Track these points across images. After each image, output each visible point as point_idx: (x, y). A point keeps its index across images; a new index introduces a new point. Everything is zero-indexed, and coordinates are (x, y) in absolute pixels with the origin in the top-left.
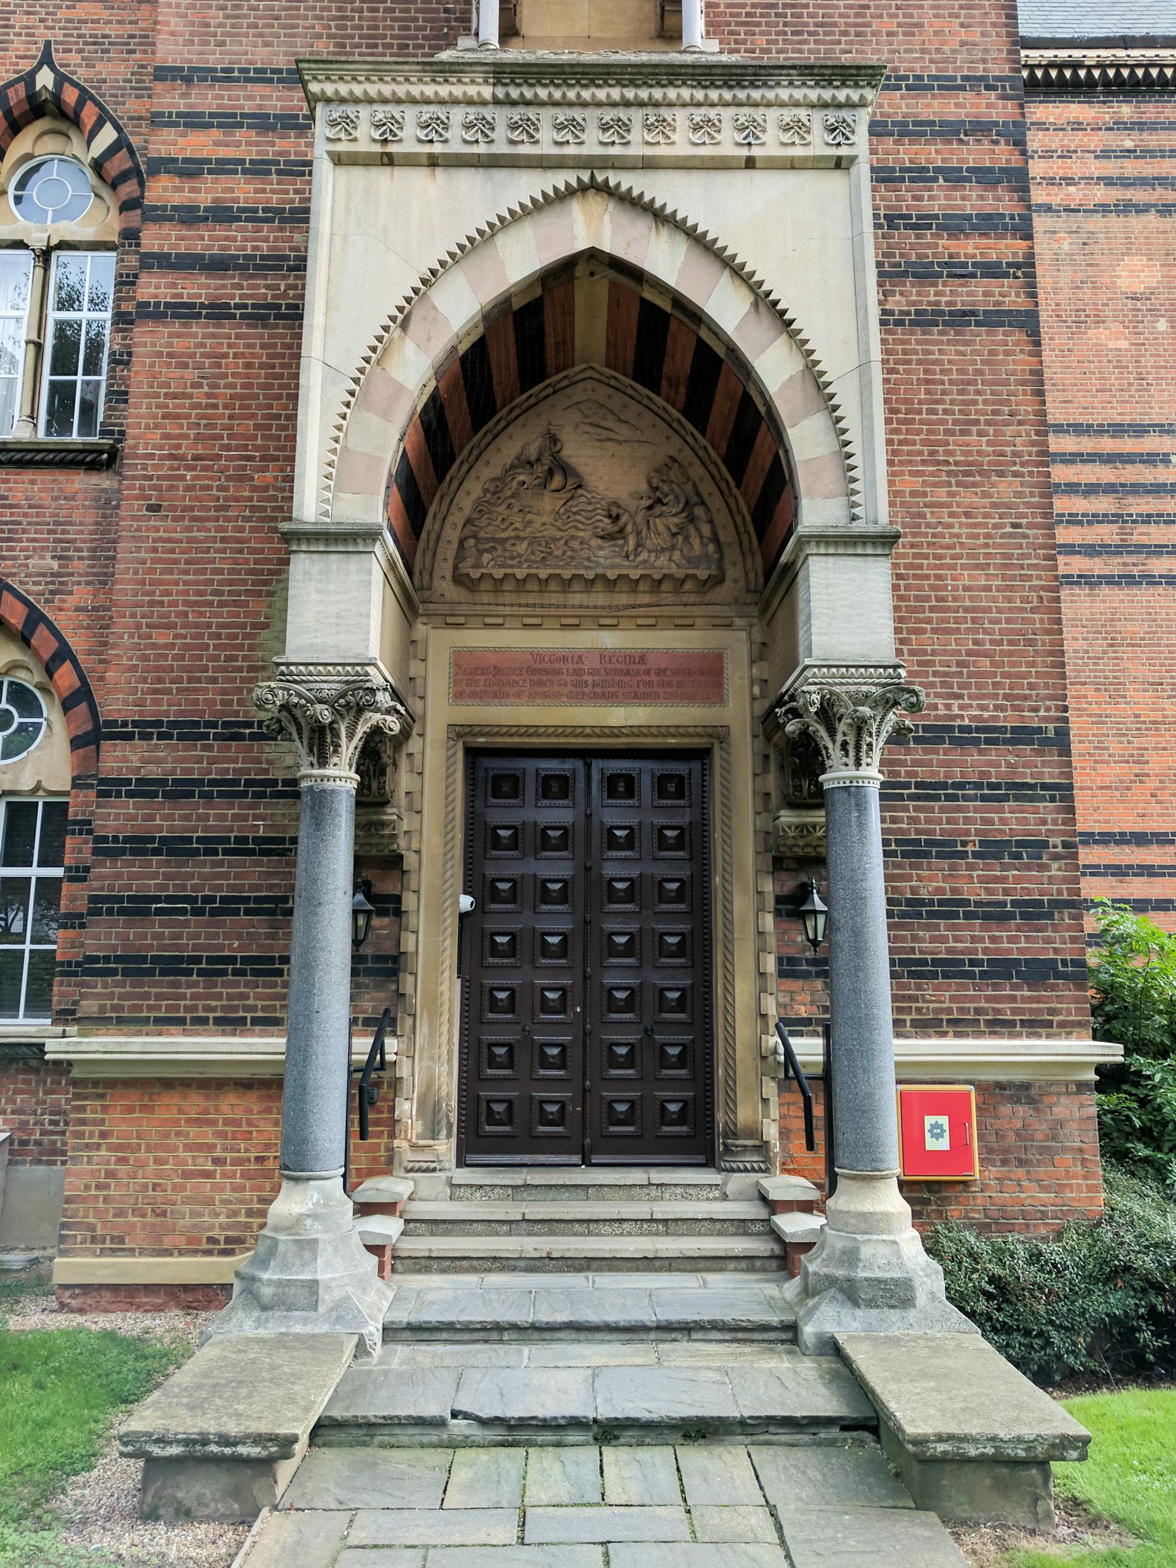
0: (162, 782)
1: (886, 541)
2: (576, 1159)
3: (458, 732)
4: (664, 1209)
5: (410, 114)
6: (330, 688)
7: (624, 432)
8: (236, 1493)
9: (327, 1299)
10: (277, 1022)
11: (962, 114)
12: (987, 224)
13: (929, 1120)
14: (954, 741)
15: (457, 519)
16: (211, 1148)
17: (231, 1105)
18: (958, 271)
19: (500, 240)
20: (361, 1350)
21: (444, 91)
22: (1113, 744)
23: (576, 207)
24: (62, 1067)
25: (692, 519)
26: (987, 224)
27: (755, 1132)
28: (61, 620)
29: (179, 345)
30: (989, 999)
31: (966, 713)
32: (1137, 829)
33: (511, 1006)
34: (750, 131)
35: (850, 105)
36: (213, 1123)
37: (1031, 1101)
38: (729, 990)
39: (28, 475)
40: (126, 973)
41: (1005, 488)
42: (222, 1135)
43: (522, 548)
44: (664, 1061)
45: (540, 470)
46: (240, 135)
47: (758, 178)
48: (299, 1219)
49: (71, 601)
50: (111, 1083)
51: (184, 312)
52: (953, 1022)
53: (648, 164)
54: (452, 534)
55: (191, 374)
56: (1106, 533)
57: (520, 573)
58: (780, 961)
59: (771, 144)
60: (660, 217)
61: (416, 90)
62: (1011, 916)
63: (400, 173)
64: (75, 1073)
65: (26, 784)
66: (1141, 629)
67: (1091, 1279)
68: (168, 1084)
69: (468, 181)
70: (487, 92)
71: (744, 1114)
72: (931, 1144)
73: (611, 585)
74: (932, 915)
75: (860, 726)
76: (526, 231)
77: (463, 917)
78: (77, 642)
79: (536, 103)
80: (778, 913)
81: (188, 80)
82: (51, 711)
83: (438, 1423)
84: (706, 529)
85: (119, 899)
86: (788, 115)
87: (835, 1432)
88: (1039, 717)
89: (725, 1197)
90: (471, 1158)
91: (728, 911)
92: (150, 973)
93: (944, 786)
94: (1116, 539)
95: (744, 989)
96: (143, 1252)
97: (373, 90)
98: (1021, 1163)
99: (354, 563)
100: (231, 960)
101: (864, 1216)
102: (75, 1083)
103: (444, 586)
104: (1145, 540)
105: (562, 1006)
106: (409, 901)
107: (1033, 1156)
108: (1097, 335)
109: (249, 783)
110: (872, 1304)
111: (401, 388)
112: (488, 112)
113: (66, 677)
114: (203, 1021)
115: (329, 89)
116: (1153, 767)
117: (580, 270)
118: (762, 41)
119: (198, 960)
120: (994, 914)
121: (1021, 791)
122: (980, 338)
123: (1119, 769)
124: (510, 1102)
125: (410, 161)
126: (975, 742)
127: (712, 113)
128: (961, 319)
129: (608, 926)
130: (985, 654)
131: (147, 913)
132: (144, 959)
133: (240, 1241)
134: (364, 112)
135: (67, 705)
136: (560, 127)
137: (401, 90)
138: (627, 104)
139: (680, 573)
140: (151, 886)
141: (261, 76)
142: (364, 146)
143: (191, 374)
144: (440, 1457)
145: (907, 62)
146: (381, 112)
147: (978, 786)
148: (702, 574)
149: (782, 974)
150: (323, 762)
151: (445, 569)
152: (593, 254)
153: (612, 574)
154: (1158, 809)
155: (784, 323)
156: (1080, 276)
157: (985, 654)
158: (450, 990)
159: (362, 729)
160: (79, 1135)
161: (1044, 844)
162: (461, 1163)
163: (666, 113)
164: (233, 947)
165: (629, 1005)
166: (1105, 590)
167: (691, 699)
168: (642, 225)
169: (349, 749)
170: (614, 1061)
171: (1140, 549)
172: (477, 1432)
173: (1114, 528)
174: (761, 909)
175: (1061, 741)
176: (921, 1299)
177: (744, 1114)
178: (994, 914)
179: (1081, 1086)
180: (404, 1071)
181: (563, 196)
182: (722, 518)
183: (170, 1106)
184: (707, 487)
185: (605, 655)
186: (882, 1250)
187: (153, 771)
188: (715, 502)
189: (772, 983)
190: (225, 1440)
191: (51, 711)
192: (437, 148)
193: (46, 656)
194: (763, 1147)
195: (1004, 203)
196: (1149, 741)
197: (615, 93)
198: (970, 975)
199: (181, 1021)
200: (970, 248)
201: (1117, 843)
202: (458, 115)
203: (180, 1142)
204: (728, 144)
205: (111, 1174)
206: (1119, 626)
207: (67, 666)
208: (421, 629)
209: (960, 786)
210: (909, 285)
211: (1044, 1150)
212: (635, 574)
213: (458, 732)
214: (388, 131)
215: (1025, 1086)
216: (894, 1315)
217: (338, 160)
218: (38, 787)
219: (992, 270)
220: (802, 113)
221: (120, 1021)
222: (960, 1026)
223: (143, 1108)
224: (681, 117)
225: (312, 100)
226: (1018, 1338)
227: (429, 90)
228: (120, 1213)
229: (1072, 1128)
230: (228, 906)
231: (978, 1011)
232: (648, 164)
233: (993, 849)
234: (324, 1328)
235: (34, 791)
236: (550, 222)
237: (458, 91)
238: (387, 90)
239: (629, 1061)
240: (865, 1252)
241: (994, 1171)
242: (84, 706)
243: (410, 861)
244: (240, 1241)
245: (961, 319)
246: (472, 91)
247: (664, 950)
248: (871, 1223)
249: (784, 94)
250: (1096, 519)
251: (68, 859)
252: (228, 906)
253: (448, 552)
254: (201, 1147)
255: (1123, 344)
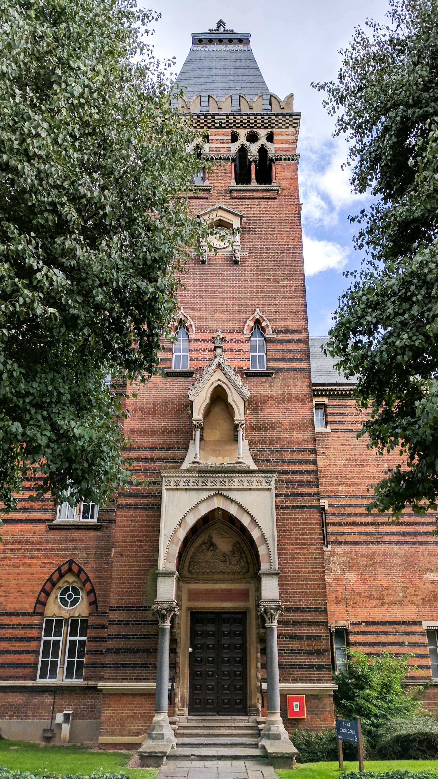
0: (123, 621)
1: (277, 574)
2: (216, 713)
3: (189, 608)
4: (234, 725)
5: (182, 480)
6: (166, 607)
7: (227, 535)
8: (157, 763)
9: (165, 738)
10: (155, 679)
11: (303, 457)
12: (309, 484)
13: (295, 703)
14: (301, 611)
15: (189, 557)
16: (133, 710)
17: (138, 700)
18: (302, 495)
19: (200, 506)
20: (173, 747)
21: (188, 475)
22: (374, 593)
23: (215, 498)
24: (101, 690)
25: (242, 557)
26: (309, 484)
27: (256, 706)
28: (87, 570)
29: (127, 515)
30: (309, 674)
31: (303, 604)
32: (382, 620)
33: (201, 675)
34: (250, 483)
35: (270, 477)
36: (134, 704)
37: (319, 699)
38: (250, 672)
39: (80, 532)
40: (115, 667)
41: (313, 549)
42: (136, 707)
43: (203, 564)
44: (236, 689)
45: (208, 545)
46: (141, 464)
47: (252, 492)
48: (160, 721)
49: (90, 566)
50: (111, 694)
51: (128, 507)
52: (301, 680)
53: (230, 490)
54: (188, 561)
55: (129, 522)
56: (371, 528)
57: (203, 571)
58: (262, 664)
59: (254, 486)
60: (233, 501)
61: (183, 475)
62: (314, 653)
63: (180, 492)
64: (104, 692)
65: (77, 614)
66: (382, 558)
67: (329, 741)
68: (124, 694)
69: (193, 493)
70: (197, 475)
71: (253, 702)
72: (295, 709)
73: (223, 573)
74: (296, 653)
75: (272, 615)
76: (205, 504)
77: (190, 653)
78: (91, 576)
79: (207, 477)
80: (261, 653)
81: (129, 451)
82: (82, 595)
83: (189, 756)
84: (245, 560)
85: (113, 649)
86: (258, 479)
87: (260, 758)
88: (320, 605)
89: (249, 722)
90: (192, 713)
91: (250, 652)
92: (120, 667)
93: (298, 622)
94: (374, 530)
95: (253, 671)
96: (118, 736)
97: (174, 475)
98: (316, 714)
99: (170, 579)
100: (138, 664)
101: (272, 721)
102: (103, 694)
103: (186, 573)
104: (382, 530)
105: (212, 675)
106: (178, 650)
107: (319, 713)
108: (367, 468)
109: (143, 621)
110: (272, 739)
111: (179, 539)
112: (197, 479)
113: (88, 586)
114: (132, 679)
115: (166, 475)
116: (386, 601)
117: (216, 511)
118: (258, 440)
119: (130, 664)
120: (310, 653)
121: (316, 623)
122: (307, 511)
123: (376, 601)
124: (200, 699)
125: (182, 489)
126: (306, 611)
127: (243, 479)
128: (303, 507)
129: (223, 656)
130: (308, 589)
131: (119, 653)
132: (118, 664)
133: (139, 733)
134: (172, 479)
135: (88, 594)
136: (212, 482)
137: (180, 475)
138: (225, 477)
139: (238, 570)
140: (120, 646)
141: (146, 450)
142: (172, 487)
143: (129, 522)
144: (190, 762)
145: (292, 445)
146: (176, 479)
147: (306, 622)
148: (244, 571)
149: (262, 668)
150: (164, 622)
151: (186, 569)
152: (219, 508)
153: (224, 571)
154: (388, 614)
155: (257, 524)
156: (362, 451)
157: (308, 589)
158: (187, 671)
159: (171, 615)
160: (104, 707)
161: (321, 636)
162: (189, 715)
163: (233, 479)
164: (139, 661)
165: (228, 675)
166: (371, 546)
167: (242, 601)
168: (228, 502)
169: (169, 619)
170: (224, 689)
171: (381, 533)
172: (196, 758)
173: (373, 527)
174: (257, 652)
175: (325, 611)
176: (282, 738)
177: (253, 702)
178: (310, 653)
179: (330, 695)
180: (177, 691)
181: (212, 496)
182: (249, 556)
183: (125, 700)
184: (245, 549)
185: (223, 590)
186: (275, 728)
187: (121, 618)
188: (247, 552)
189: (260, 670)
190: (155, 753)
191: (82, 595)
192: (187, 487)
193: (83, 580)
194: (257, 710)
195: (312, 479)
196: (385, 593)
197: (223, 475)
198: (304, 668)
199: (127, 679)
200: (305, 490)
201: (377, 625)
202: (191, 480)
203: (127, 709)
204: (246, 485)
205: (111, 716)
206: (376, 557)
207: (88, 583)
208: (181, 584)
209: (302, 622)
210: (291, 499)
211: (322, 711)
212: (229, 571)
213: (189, 608)
214: (177, 483)
215: (317, 695)
216: (277, 741)
217: (167, 489)
218: (80, 615)
219: (310, 495)
220: (261, 479)
221: (113, 679)
222: (302, 681)
223: (119, 700)
224: (236, 480)
225: (162, 477)
226: (311, 754)
227: (186, 475)
228: (113, 726)
229: (328, 706)
230: (138, 651)
231: (307, 677)
232: (230, 490)
233: (310, 637)
234: (165, 743)
235: (78, 616)
236: (210, 502)
237: (191, 475)
238: (177, 475)
239: (228, 689)
240: (272, 728)
241: (310, 716)
242: (93, 594)
243: (178, 640)
244: (139, 733)
245: (303, 507)
246: (194, 475)
247: (236, 662)
248: (273, 722)
249: (257, 475)
250: (368, 524)
251: (88, 635)
252: (138, 651)
253: (187, 565)
254: (131, 710)
255: (375, 471)
